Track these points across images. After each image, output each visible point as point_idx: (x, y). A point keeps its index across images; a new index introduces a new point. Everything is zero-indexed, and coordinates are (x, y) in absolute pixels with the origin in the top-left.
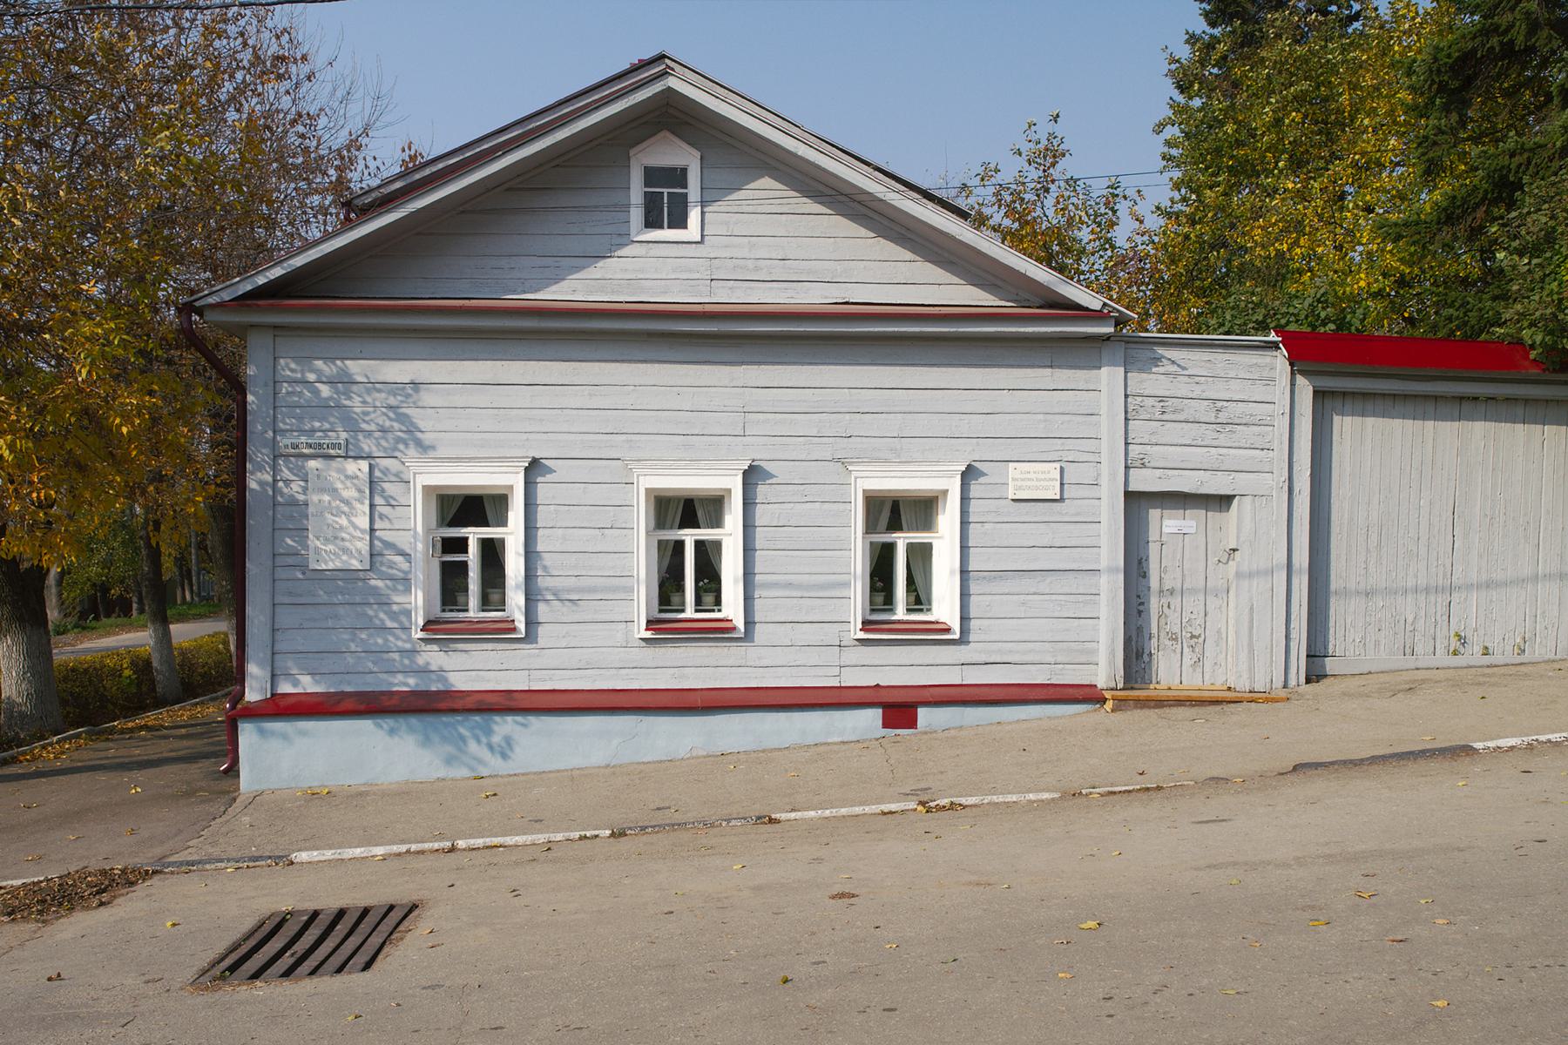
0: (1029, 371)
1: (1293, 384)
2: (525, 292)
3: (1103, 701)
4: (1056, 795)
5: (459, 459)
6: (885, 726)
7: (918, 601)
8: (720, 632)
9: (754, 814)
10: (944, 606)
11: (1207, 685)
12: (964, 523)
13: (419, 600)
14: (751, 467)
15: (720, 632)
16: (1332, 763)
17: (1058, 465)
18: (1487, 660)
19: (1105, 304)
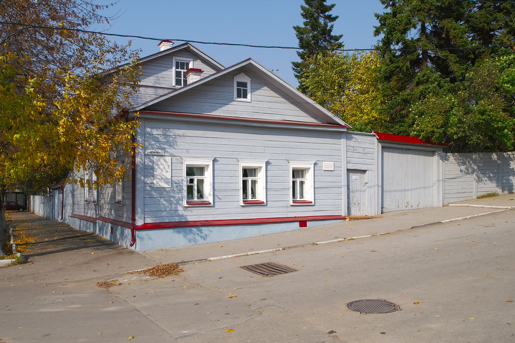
2: (208, 113)
5: (197, 157)
6: (300, 226)
9: (312, 243)
15: (260, 204)
16: (419, 226)
18: (412, 208)
19: (345, 124)
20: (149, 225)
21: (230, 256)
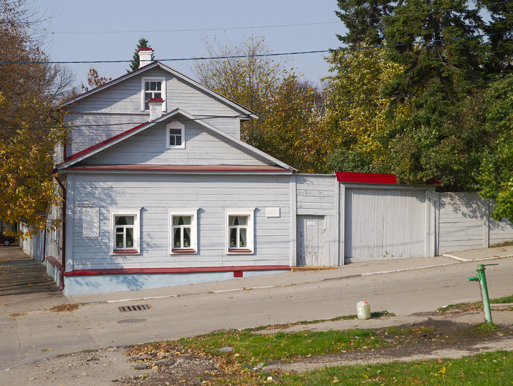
0: (271, 184)
1: (339, 186)
3: (290, 269)
4: (273, 286)
6: (235, 276)
7: (243, 244)
8: (191, 252)
10: (250, 245)
11: (319, 265)
12: (255, 223)
13: (112, 244)
14: (199, 209)
15: (191, 252)
17: (279, 208)
20: (76, 272)
21: (127, 300)
